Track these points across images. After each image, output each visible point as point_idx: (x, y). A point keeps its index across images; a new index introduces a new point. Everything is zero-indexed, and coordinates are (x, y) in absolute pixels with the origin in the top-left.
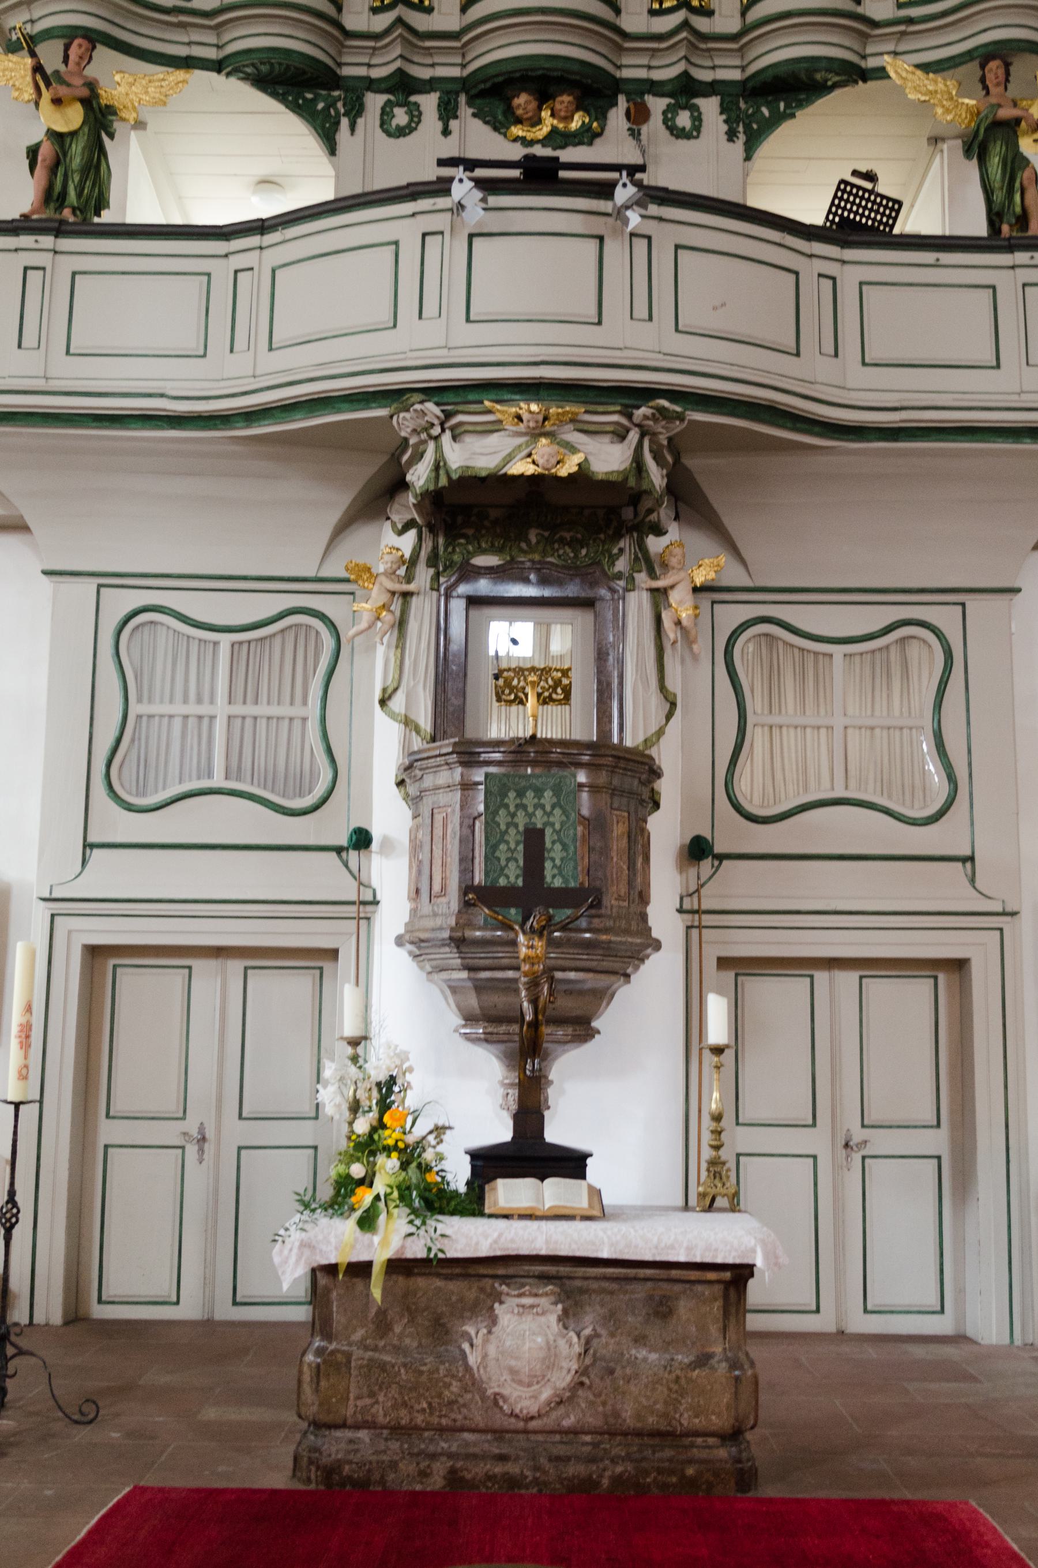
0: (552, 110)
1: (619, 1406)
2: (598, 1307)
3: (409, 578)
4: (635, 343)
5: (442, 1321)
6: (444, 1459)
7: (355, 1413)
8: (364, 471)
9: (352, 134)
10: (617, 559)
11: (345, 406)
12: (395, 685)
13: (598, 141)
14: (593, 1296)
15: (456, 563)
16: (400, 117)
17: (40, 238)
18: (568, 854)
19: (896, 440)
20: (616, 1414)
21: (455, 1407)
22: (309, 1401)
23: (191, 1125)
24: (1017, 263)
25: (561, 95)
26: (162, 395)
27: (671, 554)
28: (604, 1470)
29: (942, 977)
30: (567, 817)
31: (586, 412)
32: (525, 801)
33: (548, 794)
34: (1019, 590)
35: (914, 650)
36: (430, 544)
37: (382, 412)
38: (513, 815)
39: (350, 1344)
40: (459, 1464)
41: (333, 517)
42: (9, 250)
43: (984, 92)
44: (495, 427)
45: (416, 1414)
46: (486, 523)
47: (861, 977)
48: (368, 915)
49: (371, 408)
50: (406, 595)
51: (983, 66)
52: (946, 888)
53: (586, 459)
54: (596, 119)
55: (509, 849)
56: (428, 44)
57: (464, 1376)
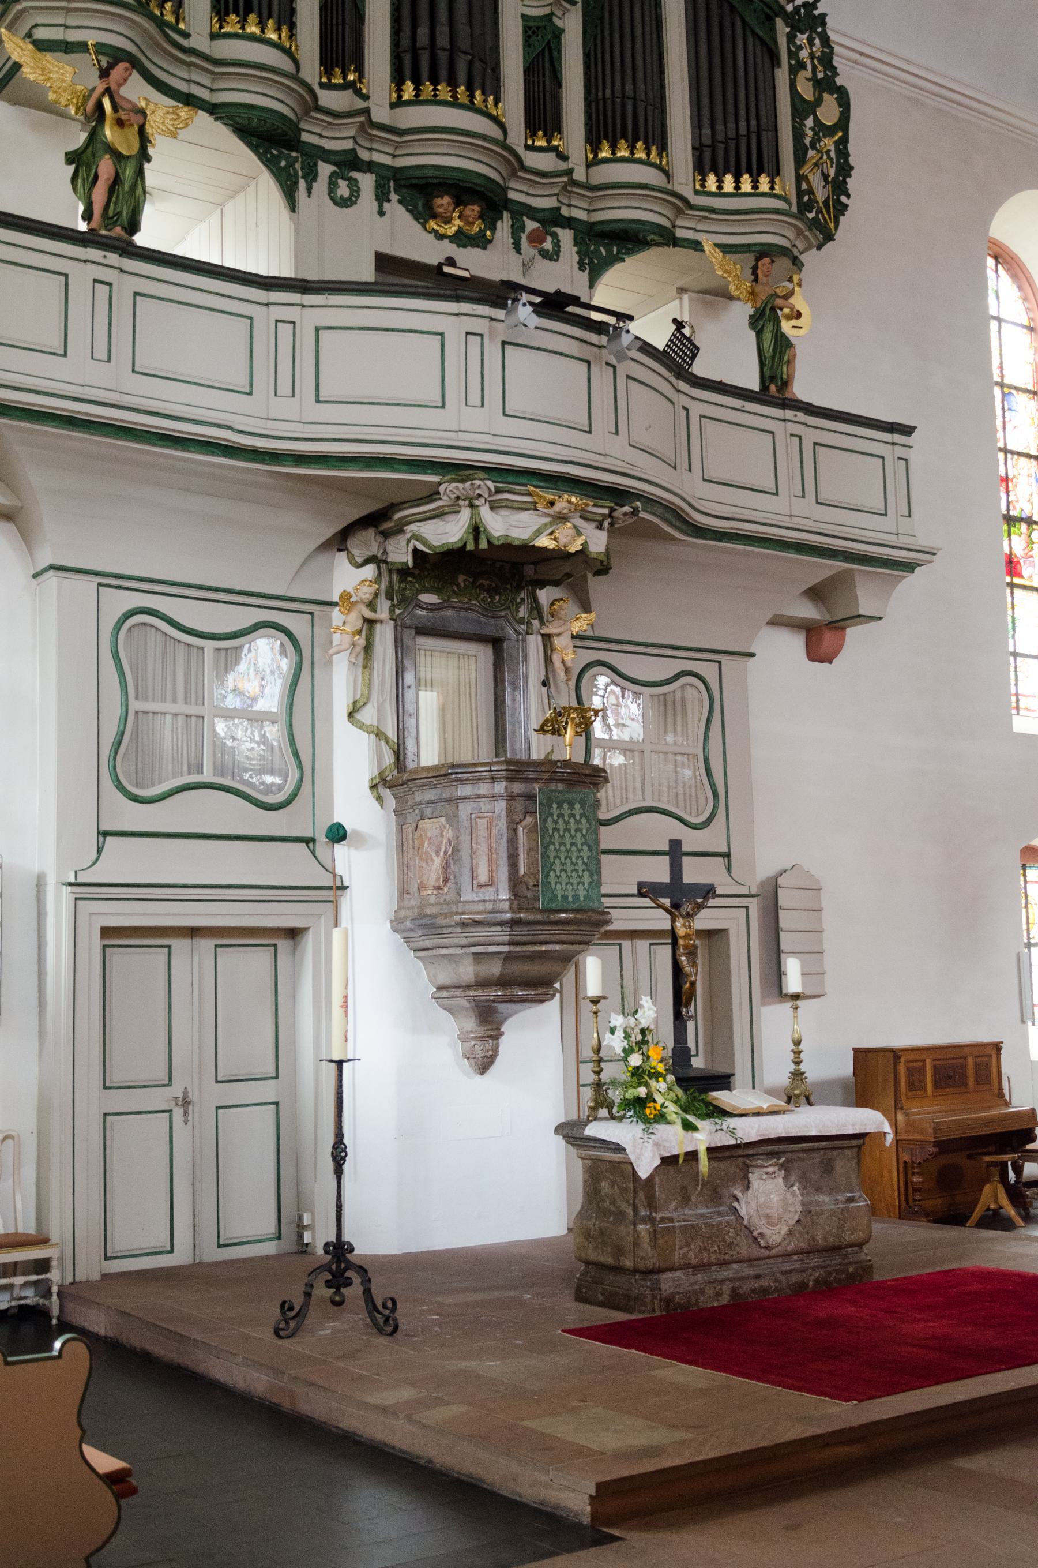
0: (461, 213)
4: (609, 453)
6: (728, 1283)
9: (309, 197)
11: (404, 467)
12: (365, 700)
13: (489, 246)
16: (343, 190)
17: (108, 254)
19: (720, 541)
20: (814, 1239)
23: (176, 1090)
25: (473, 204)
26: (229, 428)
27: (560, 607)
33: (577, 806)
34: (753, 655)
37: (434, 479)
38: (556, 822)
40: (737, 1284)
42: (80, 260)
43: (753, 277)
46: (428, 566)
50: (370, 623)
51: (758, 259)
54: (490, 229)
56: (376, 132)
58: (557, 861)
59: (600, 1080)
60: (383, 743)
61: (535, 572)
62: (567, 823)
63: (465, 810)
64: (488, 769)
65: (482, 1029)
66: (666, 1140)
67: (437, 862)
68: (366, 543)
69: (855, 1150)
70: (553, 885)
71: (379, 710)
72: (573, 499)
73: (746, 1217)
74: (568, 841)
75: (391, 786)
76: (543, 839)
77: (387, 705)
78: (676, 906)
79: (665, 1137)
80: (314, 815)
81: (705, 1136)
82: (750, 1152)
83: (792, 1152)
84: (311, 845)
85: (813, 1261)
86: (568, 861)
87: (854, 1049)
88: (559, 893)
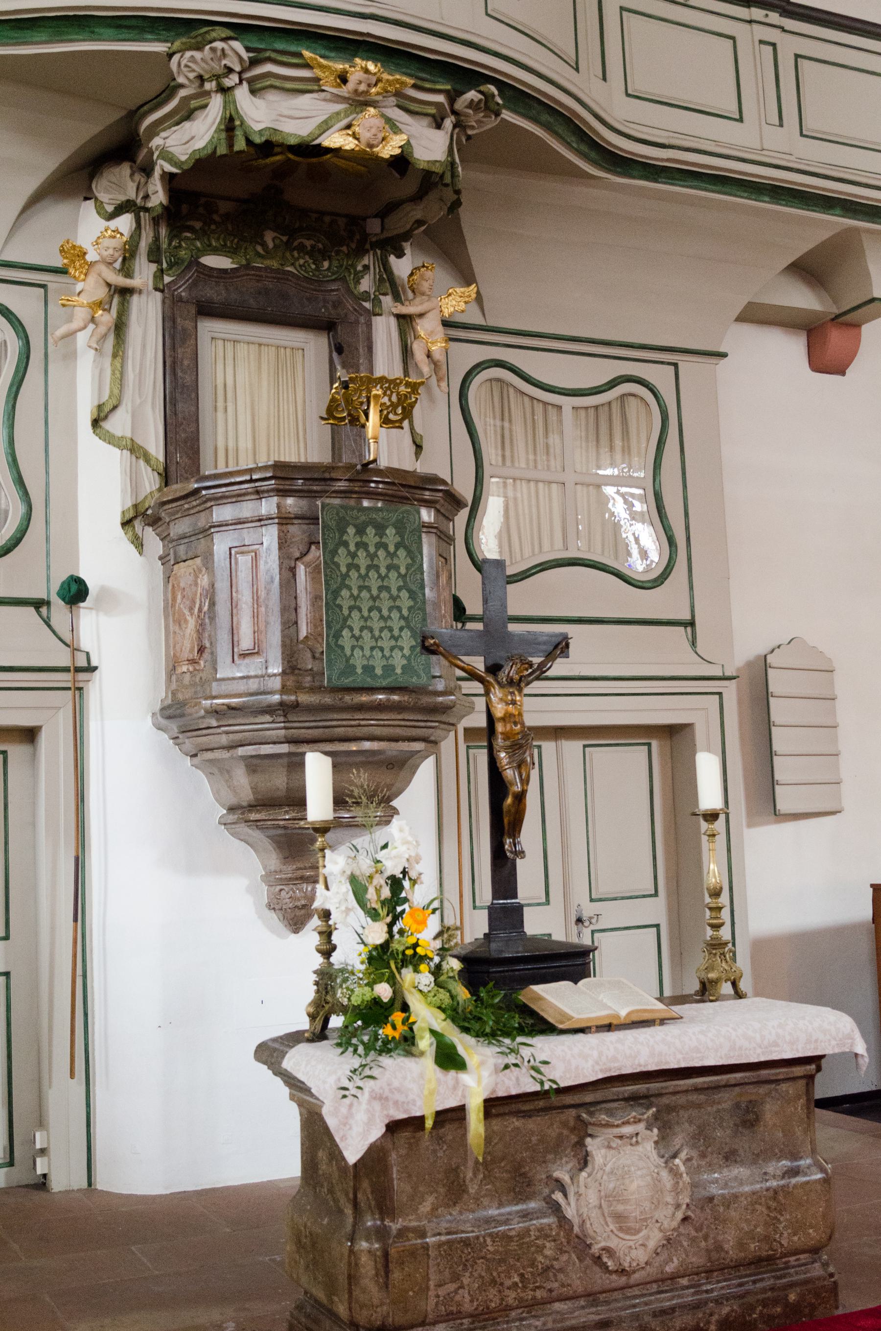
1: (720, 1238)
2: (687, 1125)
3: (126, 270)
5: (523, 1170)
7: (437, 1304)
8: (85, 129)
10: (362, 277)
11: (110, 32)
12: (115, 402)
14: (682, 1112)
15: (183, 261)
18: (416, 603)
20: (719, 1248)
21: (551, 1274)
22: (376, 1301)
24: (754, 18)
27: (422, 277)
28: (711, 1315)
29: (655, 744)
30: (412, 559)
31: (415, 86)
32: (365, 539)
33: (390, 531)
34: (724, 355)
35: (633, 405)
36: (151, 234)
37: (160, 47)
38: (354, 555)
39: (419, 1219)
41: (31, 184)
44: (313, 86)
45: (507, 1292)
46: (216, 217)
47: (585, 746)
48: (81, 685)
49: (146, 40)
50: (125, 292)
52: (667, 652)
53: (408, 143)
55: (352, 595)
57: (558, 1234)
58: (355, 614)
59: (331, 965)
60: (142, 462)
61: (383, 228)
62: (372, 556)
63: (221, 544)
64: (248, 478)
65: (290, 868)
66: (398, 1090)
67: (192, 622)
68: (117, 183)
69: (802, 1082)
70: (348, 652)
71: (133, 416)
72: (371, 66)
73: (576, 1221)
74: (374, 582)
75: (154, 521)
76: (332, 582)
77: (148, 409)
78: (494, 669)
79: (396, 1084)
80: (48, 567)
81: (485, 1073)
82: (589, 1098)
83: (675, 1093)
84: (44, 610)
85: (716, 1287)
86: (375, 614)
87: (872, 886)
88: (358, 662)
